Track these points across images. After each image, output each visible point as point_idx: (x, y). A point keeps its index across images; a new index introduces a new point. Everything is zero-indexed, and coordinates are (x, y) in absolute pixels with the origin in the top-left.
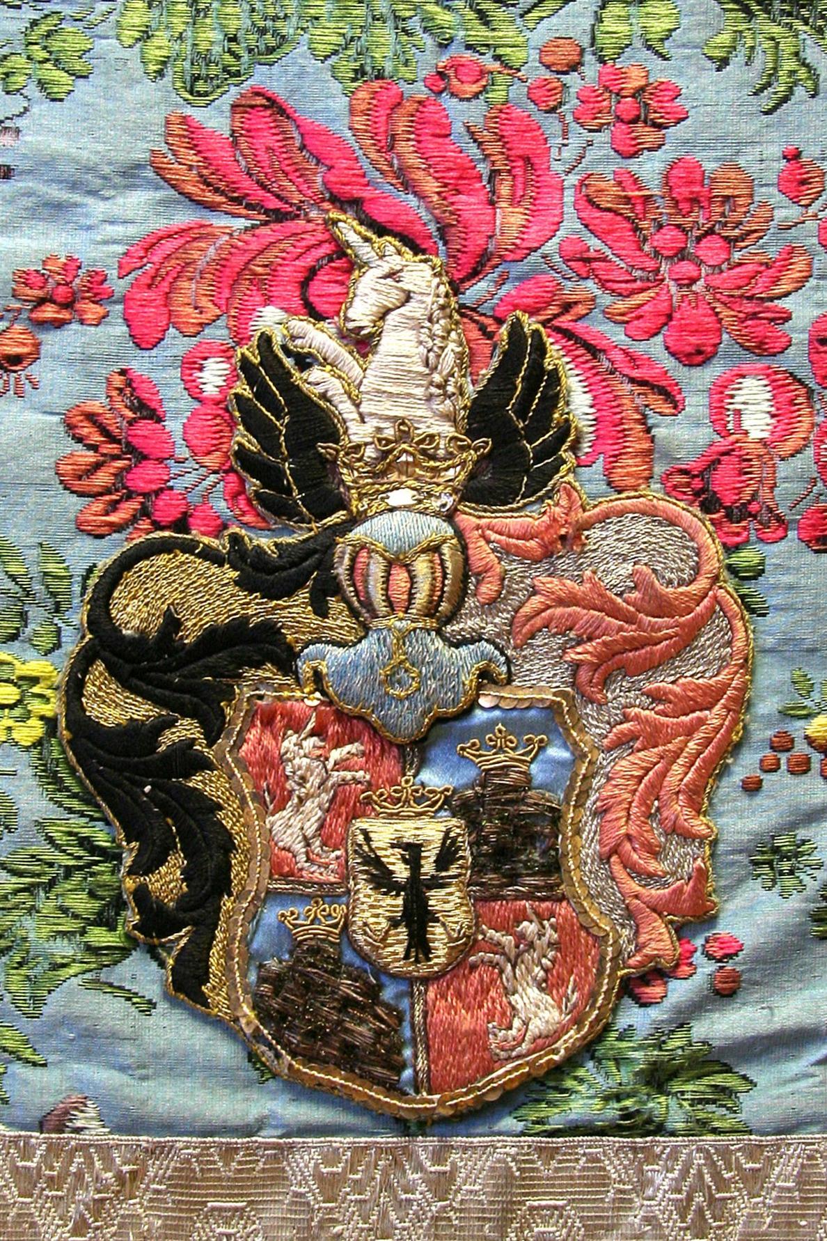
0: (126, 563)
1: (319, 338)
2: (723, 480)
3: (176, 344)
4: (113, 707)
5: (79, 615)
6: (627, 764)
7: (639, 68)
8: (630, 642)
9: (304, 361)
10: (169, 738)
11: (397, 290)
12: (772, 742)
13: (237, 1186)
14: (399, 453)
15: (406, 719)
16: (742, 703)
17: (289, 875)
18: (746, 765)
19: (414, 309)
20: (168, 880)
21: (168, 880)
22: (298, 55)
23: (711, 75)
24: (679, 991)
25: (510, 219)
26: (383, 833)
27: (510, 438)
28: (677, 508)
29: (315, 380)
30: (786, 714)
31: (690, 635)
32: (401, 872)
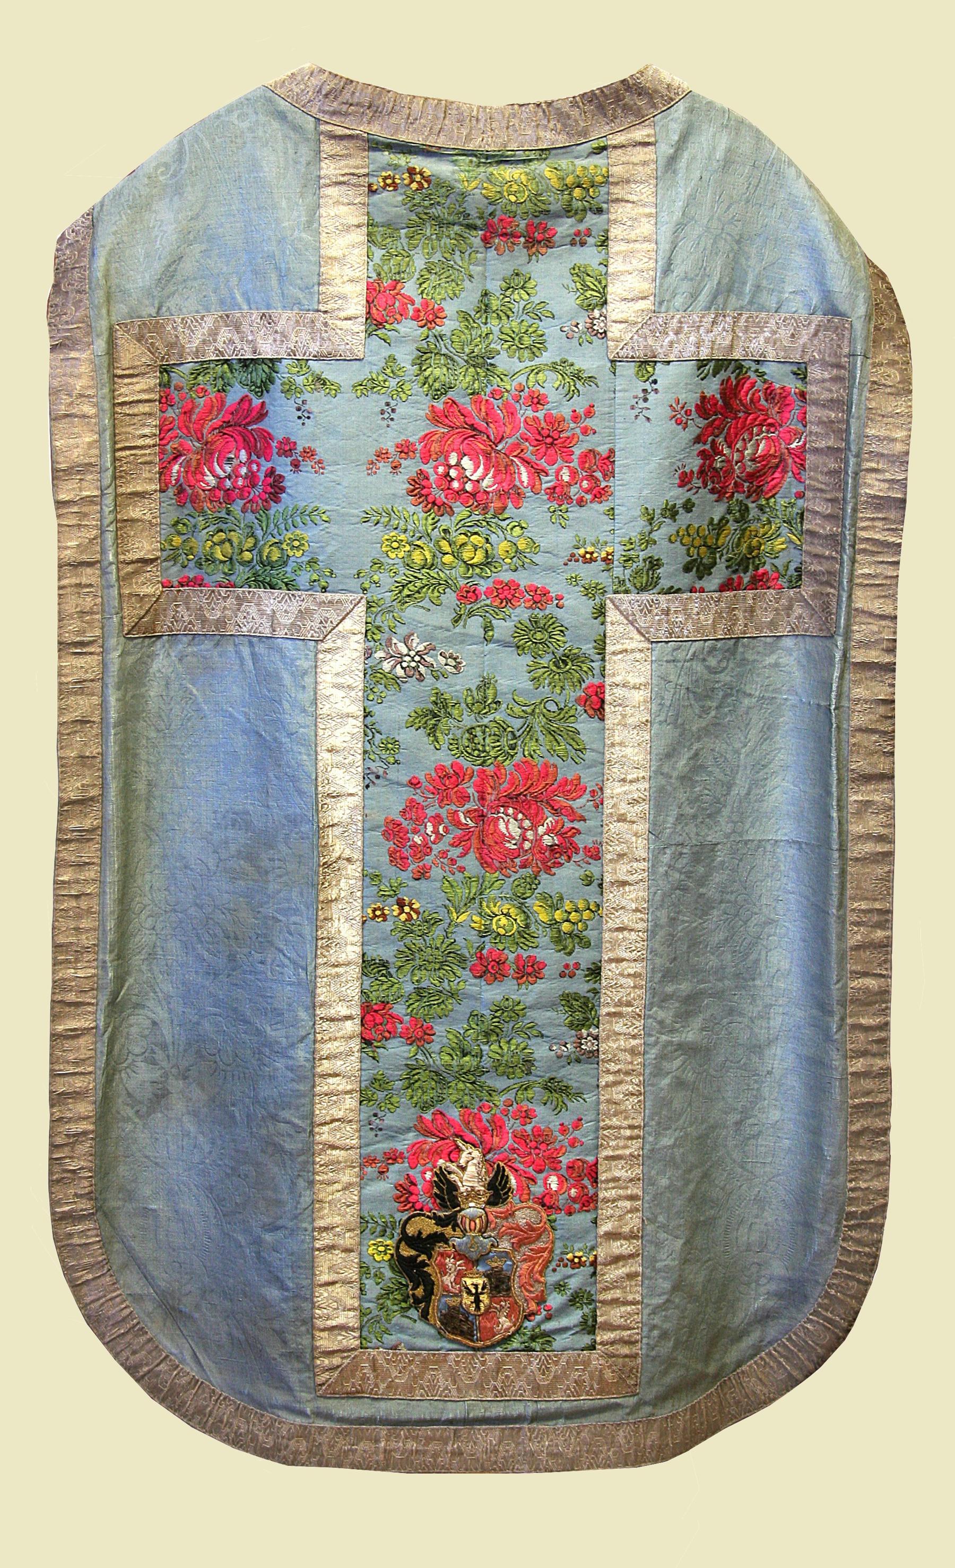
0: (409, 1218)
1: (453, 1167)
2: (546, 1200)
3: (420, 1168)
4: (407, 1252)
5: (399, 1231)
6: (525, 1266)
7: (526, 1105)
8: (526, 1236)
9: (450, 1173)
10: (420, 1259)
11: (471, 1156)
12: (581, 306)
13: (435, 1363)
14: (473, 1194)
15: (474, 1256)
16: (552, 1251)
17: (448, 1291)
18: (553, 1265)
19: (475, 1161)
20: (420, 1291)
21: (420, 1291)
22: (447, 1102)
23: (543, 1107)
24: (538, 1318)
25: (496, 1140)
26: (469, 1282)
27: (497, 1190)
28: (536, 1206)
29: (453, 1177)
30: (562, 1253)
31: (540, 1235)
32: (474, 1291)
